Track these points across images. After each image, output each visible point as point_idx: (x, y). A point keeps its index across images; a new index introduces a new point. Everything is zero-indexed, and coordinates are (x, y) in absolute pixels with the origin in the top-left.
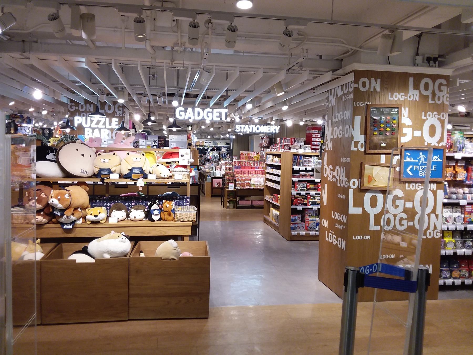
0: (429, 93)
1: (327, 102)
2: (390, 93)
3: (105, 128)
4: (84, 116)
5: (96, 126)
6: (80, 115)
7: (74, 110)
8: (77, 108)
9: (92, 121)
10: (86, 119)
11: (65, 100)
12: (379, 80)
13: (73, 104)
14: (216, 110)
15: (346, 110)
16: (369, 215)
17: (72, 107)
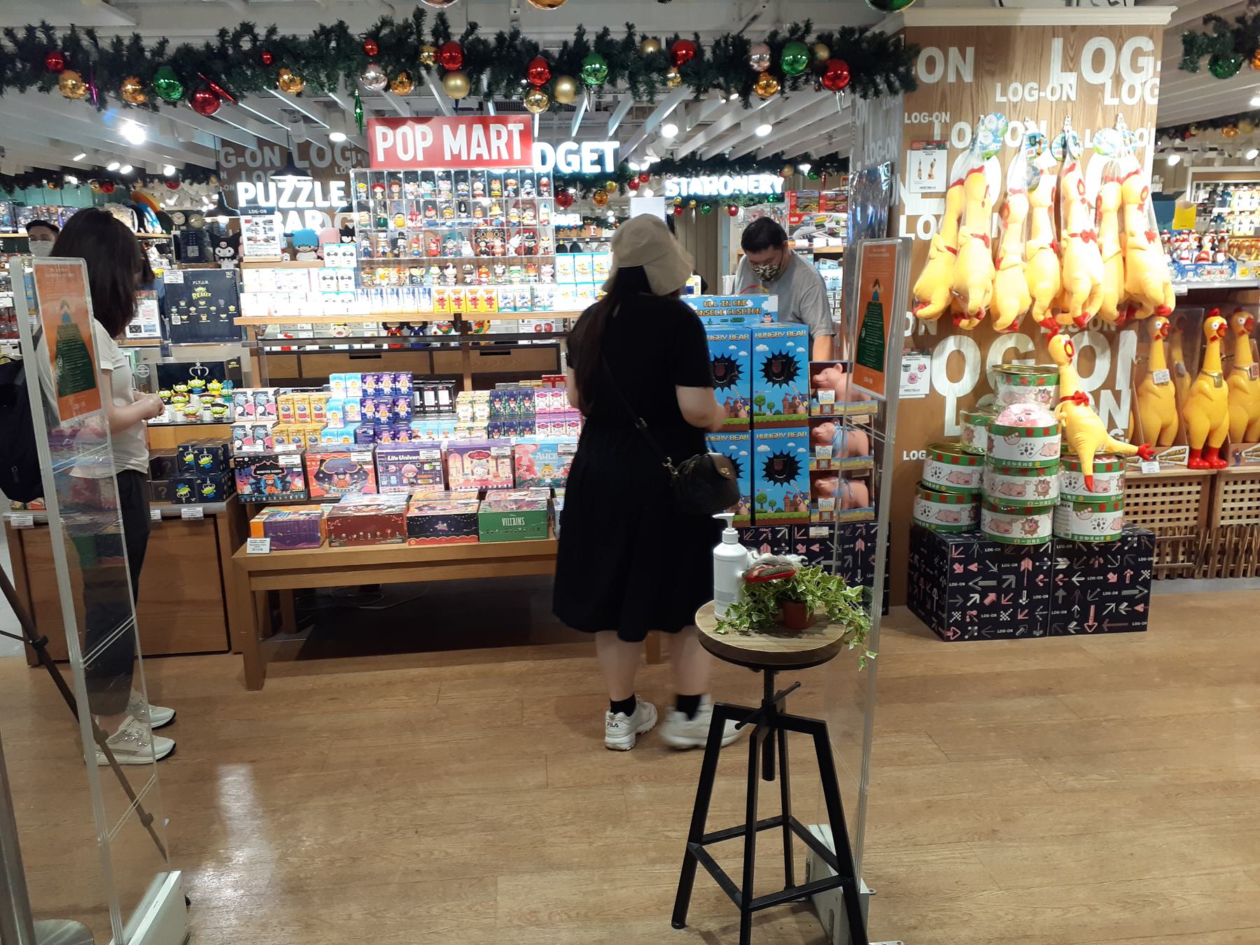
0: (1105, 77)
1: (853, 114)
2: (999, 85)
3: (315, 208)
4: (259, 178)
5: (292, 205)
6: (249, 179)
7: (233, 164)
8: (241, 160)
9: (280, 192)
10: (266, 186)
11: (209, 144)
12: (970, 51)
13: (231, 151)
14: (587, 146)
15: (889, 135)
16: (942, 400)
17: (229, 158)
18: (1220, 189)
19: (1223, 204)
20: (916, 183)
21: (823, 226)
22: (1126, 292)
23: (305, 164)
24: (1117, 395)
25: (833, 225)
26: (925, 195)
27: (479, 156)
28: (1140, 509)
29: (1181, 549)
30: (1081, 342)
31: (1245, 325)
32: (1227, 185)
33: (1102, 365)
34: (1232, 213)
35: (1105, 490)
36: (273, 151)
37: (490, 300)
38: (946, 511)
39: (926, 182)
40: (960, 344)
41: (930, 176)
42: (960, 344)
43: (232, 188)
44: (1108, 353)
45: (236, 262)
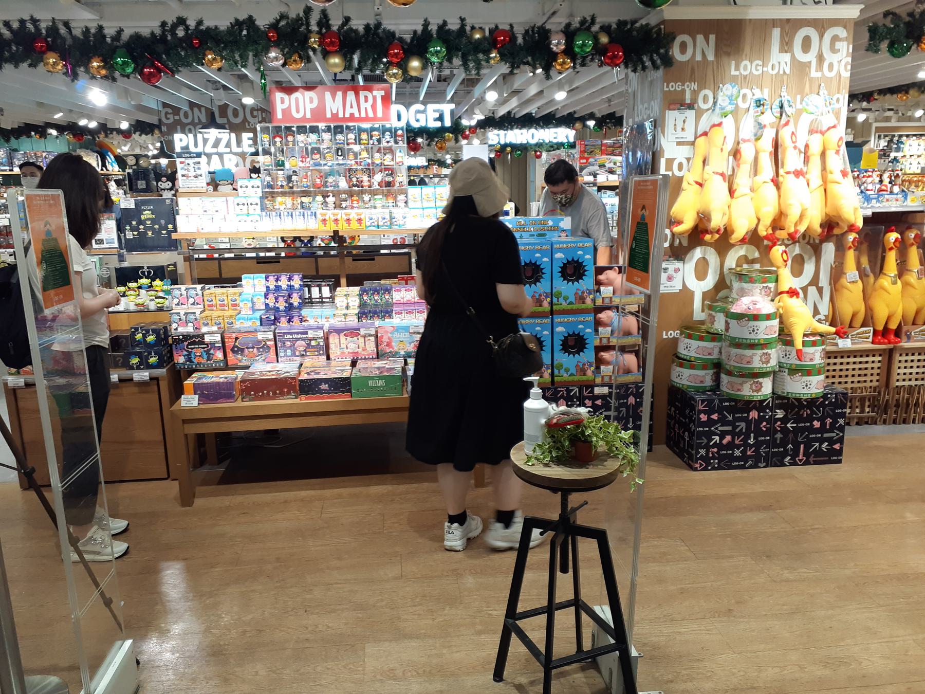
0: (811, 57)
1: (626, 84)
2: (733, 63)
3: (231, 153)
4: (190, 131)
5: (215, 150)
6: (183, 132)
7: (171, 120)
8: (177, 117)
9: (205, 141)
10: (195, 137)
11: (153, 105)
12: (712, 38)
13: (170, 111)
14: (431, 107)
15: (653, 99)
16: (692, 294)
17: (168, 116)
18: (896, 139)
19: (898, 149)
20: (672, 134)
21: (604, 166)
22: (827, 215)
23: (224, 121)
24: (820, 290)
25: (612, 165)
26: (679, 144)
27: (352, 115)
28: (837, 373)
29: (867, 403)
30: (794, 251)
31: (914, 238)
32: (900, 136)
33: (809, 268)
34: (904, 156)
35: (811, 360)
36: (200, 111)
37: (360, 220)
38: (695, 375)
39: (680, 134)
40: (705, 253)
41: (683, 129)
42: (705, 253)
43: (170, 138)
44: (814, 259)
45: (173, 192)
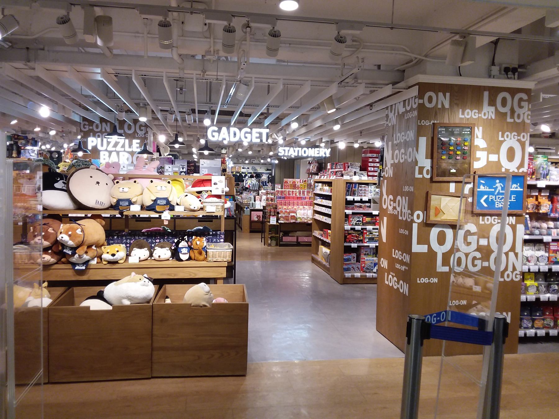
0: (507, 110)
1: (387, 121)
2: (461, 110)
3: (125, 151)
4: (99, 136)
5: (114, 149)
6: (94, 136)
7: (87, 129)
8: (91, 128)
9: (108, 143)
10: (102, 141)
11: (77, 119)
12: (448, 95)
13: (87, 123)
14: (255, 130)
15: (409, 130)
16: (436, 254)
17: (85, 126)
